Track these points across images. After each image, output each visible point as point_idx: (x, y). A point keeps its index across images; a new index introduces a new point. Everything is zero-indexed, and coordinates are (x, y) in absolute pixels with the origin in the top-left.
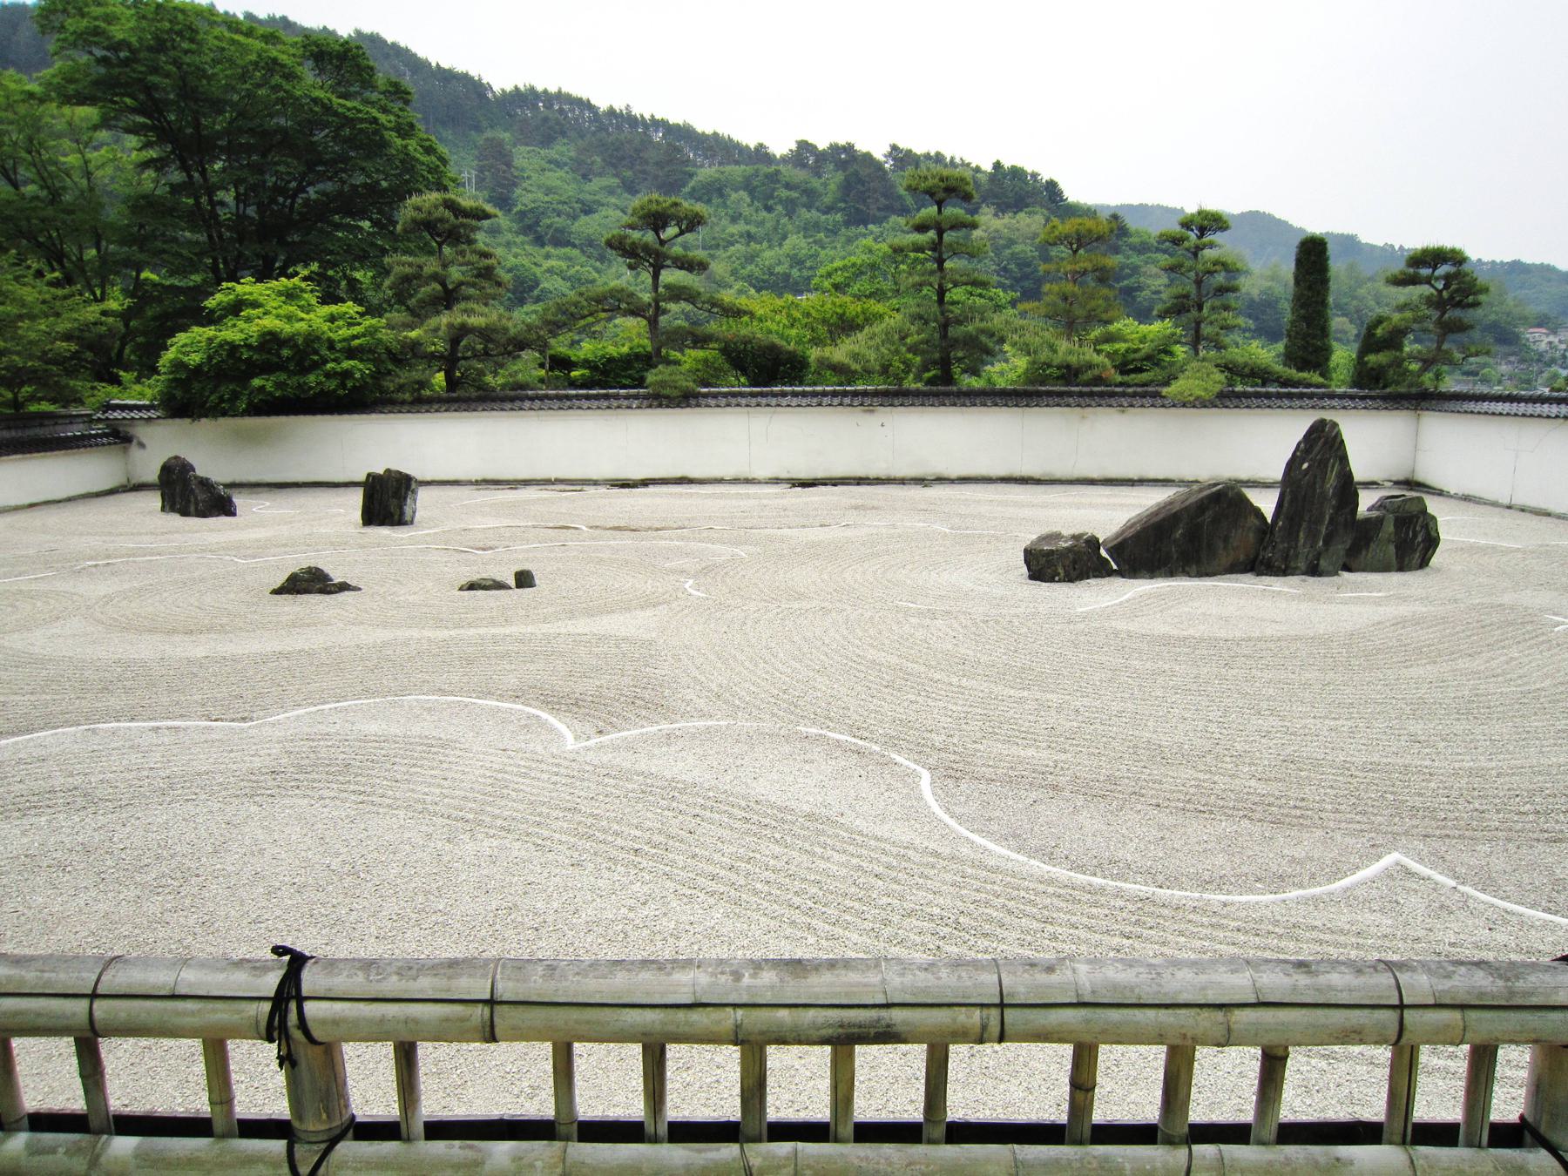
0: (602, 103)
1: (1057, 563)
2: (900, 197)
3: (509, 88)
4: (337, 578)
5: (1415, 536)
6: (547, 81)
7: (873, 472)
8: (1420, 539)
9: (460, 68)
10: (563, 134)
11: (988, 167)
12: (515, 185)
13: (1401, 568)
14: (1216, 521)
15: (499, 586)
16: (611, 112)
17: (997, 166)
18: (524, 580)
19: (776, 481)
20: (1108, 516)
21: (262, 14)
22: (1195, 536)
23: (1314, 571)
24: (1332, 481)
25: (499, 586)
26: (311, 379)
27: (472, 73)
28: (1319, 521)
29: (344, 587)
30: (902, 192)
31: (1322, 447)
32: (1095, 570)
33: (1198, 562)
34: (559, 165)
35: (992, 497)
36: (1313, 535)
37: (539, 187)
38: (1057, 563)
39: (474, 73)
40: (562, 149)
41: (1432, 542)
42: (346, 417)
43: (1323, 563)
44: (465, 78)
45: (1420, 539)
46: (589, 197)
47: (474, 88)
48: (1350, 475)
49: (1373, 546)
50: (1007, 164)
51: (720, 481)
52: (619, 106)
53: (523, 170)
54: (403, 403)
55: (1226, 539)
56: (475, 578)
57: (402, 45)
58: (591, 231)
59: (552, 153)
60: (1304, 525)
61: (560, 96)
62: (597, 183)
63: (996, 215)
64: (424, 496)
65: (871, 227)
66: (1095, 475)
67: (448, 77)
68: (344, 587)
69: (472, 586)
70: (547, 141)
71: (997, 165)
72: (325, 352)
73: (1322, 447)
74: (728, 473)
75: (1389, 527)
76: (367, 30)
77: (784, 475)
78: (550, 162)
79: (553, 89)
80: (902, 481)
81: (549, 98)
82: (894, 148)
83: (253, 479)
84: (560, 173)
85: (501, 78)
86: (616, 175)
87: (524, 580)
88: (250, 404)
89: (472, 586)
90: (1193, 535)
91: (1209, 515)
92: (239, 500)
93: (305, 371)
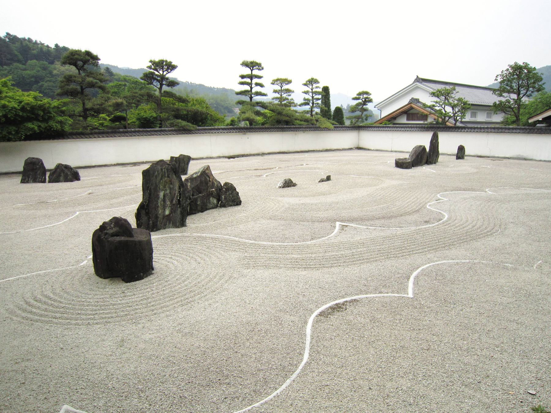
1: (400, 164)
2: (16, 55)
7: (246, 153)
11: (52, 46)
17: (57, 45)
18: (328, 178)
19: (219, 157)
30: (16, 53)
35: (352, 154)
42: (51, 141)
48: (44, 168)
50: (61, 45)
51: (202, 158)
63: (62, 65)
64: (191, 162)
65: (5, 67)
66: (299, 150)
71: (57, 45)
74: (205, 156)
77: (221, 155)
80: (254, 155)
82: (8, 34)
87: (328, 178)
88: (26, 135)
92: (81, 172)
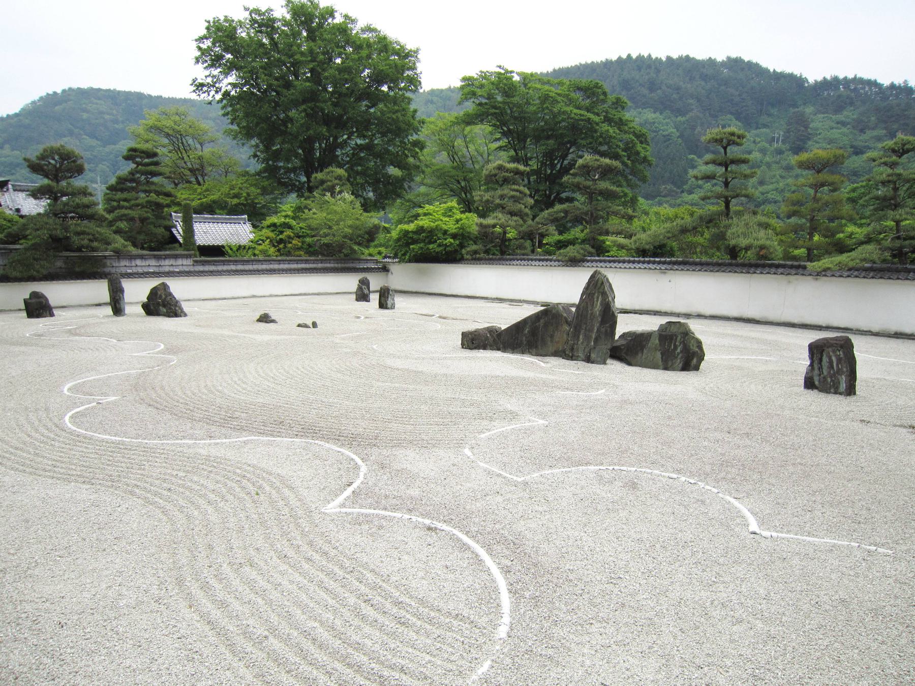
0: (885, 82)
1: (474, 341)
3: (819, 79)
4: (273, 318)
5: (676, 347)
6: (845, 71)
8: (679, 350)
9: (788, 70)
10: (852, 104)
12: (809, 139)
13: (666, 368)
14: (546, 325)
15: (306, 326)
16: (892, 86)
20: (506, 318)
21: (675, 56)
22: (536, 335)
23: (588, 360)
24: (598, 308)
25: (306, 326)
26: (431, 246)
27: (795, 73)
28: (591, 330)
29: (273, 321)
31: (597, 289)
32: (491, 346)
33: (536, 347)
34: (844, 124)
36: (587, 338)
37: (825, 139)
38: (474, 341)
39: (797, 72)
40: (849, 114)
41: (701, 357)
43: (593, 356)
44: (791, 77)
45: (679, 350)
46: (861, 144)
47: (796, 82)
49: (645, 351)
52: (899, 81)
53: (817, 129)
54: (467, 259)
55: (552, 336)
56: (301, 322)
57: (754, 61)
58: (856, 165)
59: (840, 117)
60: (582, 332)
61: (857, 81)
62: (869, 134)
66: (796, 321)
67: (779, 77)
68: (273, 321)
69: (299, 326)
70: (839, 109)
72: (440, 235)
73: (597, 289)
75: (655, 341)
76: (734, 56)
78: (838, 123)
79: (851, 76)
81: (846, 82)
83: (422, 290)
84: (845, 130)
85: (813, 74)
86: (885, 128)
89: (299, 326)
90: (534, 333)
91: (542, 321)
93: (430, 243)
